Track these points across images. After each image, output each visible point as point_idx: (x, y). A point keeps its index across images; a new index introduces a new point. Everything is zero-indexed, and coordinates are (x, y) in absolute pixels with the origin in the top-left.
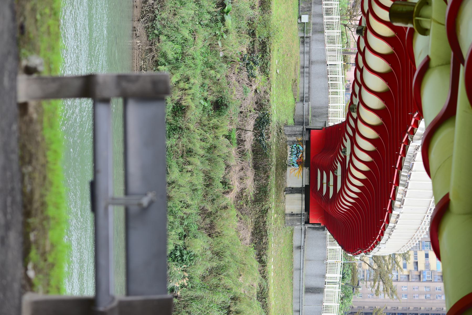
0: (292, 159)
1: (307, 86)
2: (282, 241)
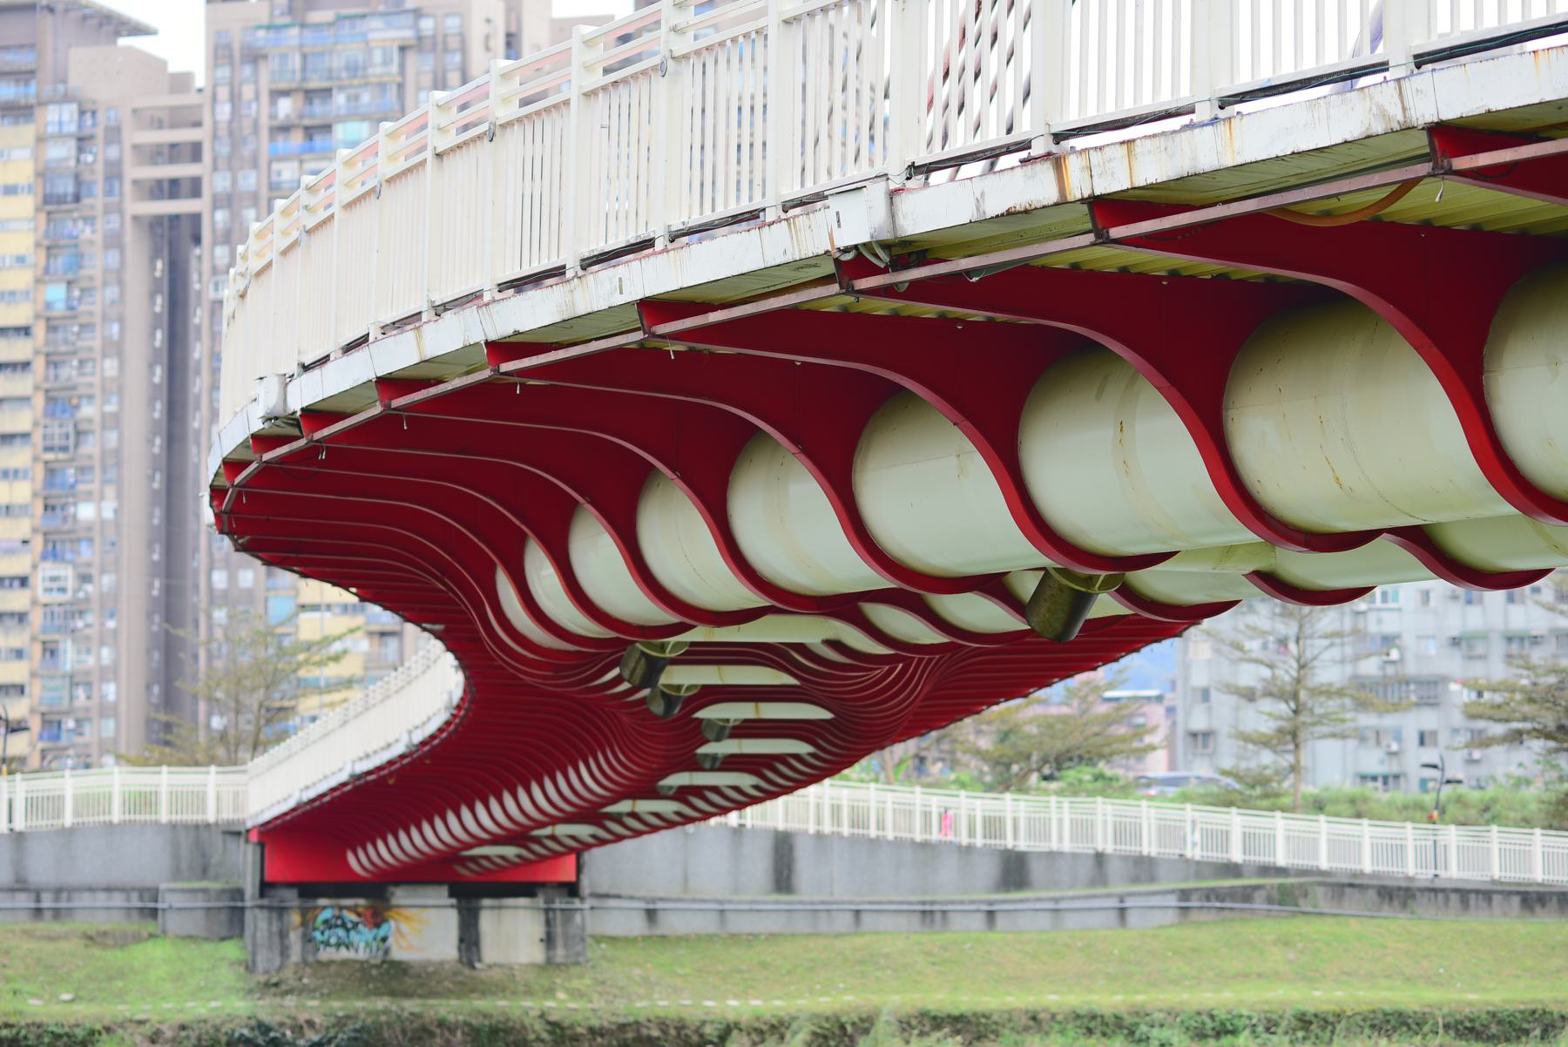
0: (362, 945)
1: (101, 896)
2: (637, 972)
